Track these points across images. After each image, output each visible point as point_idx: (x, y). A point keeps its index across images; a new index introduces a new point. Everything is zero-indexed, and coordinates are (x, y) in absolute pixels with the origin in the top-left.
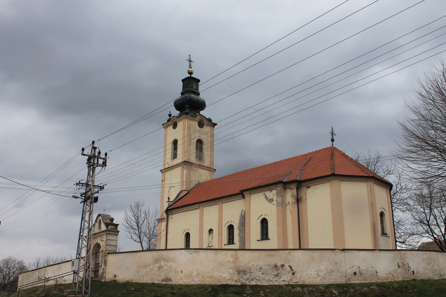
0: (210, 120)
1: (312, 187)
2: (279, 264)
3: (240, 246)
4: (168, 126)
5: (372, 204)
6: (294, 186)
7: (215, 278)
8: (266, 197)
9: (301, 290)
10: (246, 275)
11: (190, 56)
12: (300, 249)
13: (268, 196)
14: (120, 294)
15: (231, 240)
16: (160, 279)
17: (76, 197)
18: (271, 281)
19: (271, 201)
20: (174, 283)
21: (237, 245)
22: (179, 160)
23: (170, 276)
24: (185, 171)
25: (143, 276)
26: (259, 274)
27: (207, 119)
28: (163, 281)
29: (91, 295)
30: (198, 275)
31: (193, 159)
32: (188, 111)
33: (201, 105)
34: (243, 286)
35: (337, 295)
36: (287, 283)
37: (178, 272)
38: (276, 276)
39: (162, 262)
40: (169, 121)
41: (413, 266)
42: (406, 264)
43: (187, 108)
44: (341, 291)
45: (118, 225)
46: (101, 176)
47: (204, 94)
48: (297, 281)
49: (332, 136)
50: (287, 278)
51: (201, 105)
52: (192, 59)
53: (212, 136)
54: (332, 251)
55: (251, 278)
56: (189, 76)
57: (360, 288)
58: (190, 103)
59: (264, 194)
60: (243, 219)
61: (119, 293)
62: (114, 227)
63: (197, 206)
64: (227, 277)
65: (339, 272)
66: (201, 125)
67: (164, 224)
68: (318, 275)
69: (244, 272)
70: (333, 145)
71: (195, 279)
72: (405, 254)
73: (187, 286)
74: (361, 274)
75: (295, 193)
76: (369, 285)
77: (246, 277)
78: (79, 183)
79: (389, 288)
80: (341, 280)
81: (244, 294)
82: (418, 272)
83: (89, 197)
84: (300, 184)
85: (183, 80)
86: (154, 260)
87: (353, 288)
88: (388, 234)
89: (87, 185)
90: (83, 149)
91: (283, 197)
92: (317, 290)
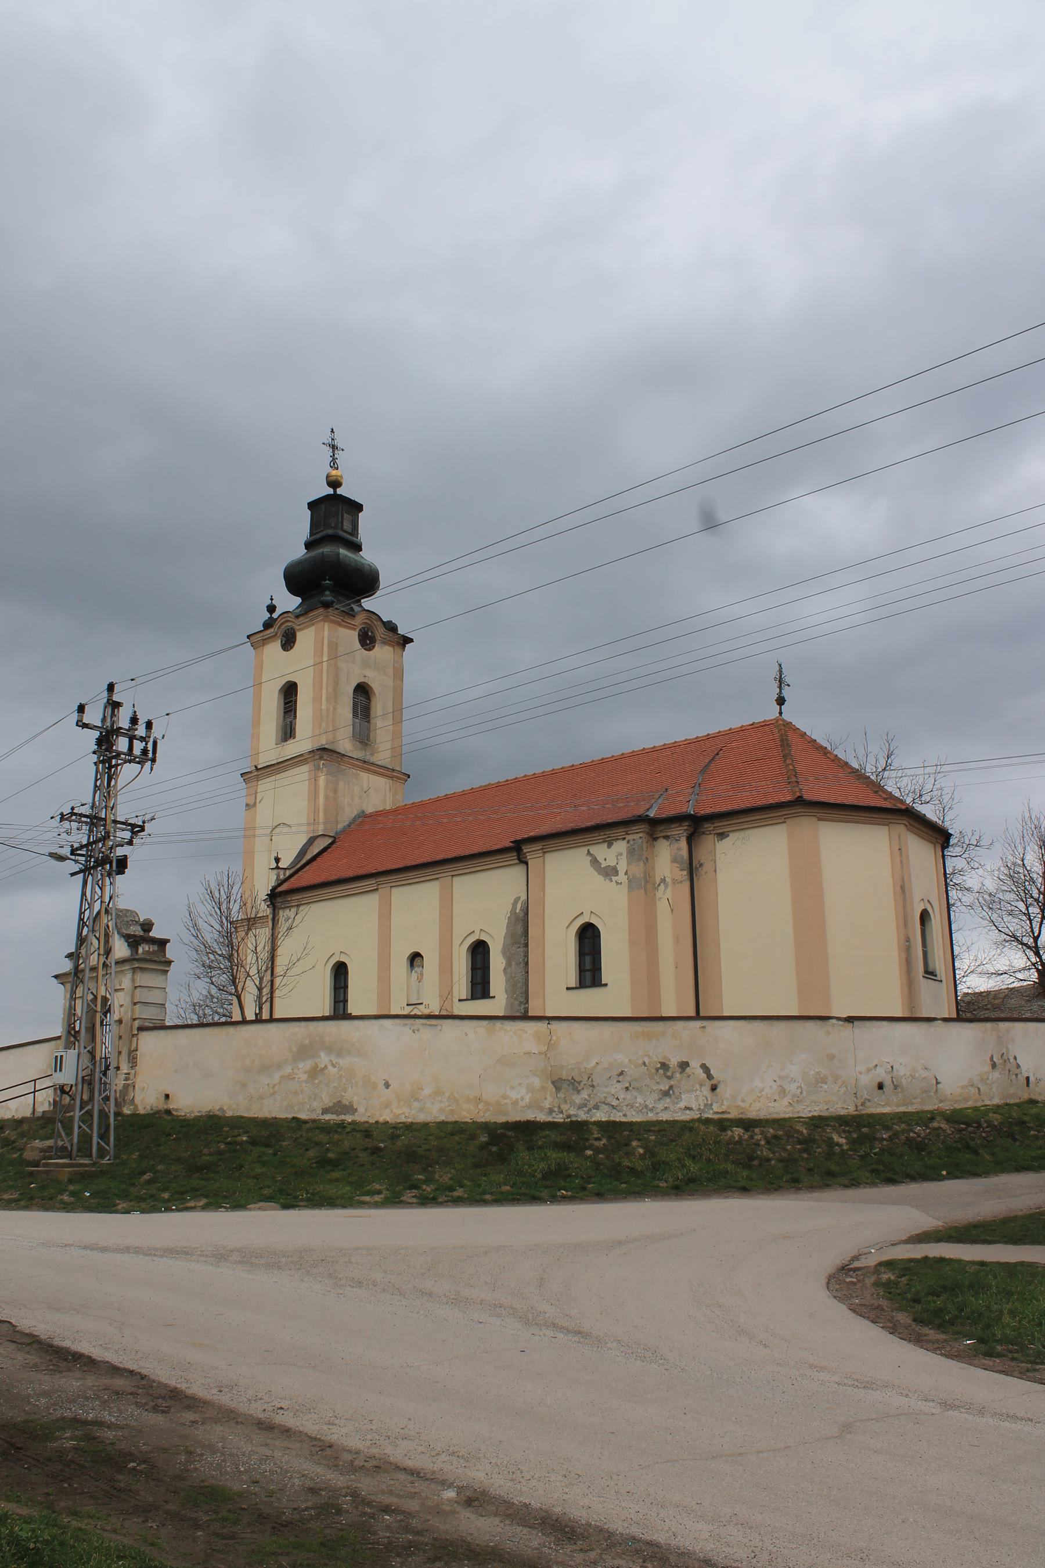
0: (391, 627)
2: (673, 1062)
3: (510, 1005)
4: (265, 641)
5: (902, 888)
6: (680, 832)
7: (487, 1103)
8: (595, 862)
9: (746, 1137)
10: (578, 1092)
11: (332, 431)
12: (698, 1017)
13: (600, 859)
14: (210, 1154)
15: (480, 987)
16: (318, 1105)
17: (61, 858)
18: (651, 1110)
19: (609, 872)
20: (364, 1119)
21: (497, 1003)
22: (303, 742)
23: (350, 1096)
24: (322, 780)
25: (261, 1098)
26: (616, 1088)
27: (383, 623)
28: (325, 1111)
29: (115, 1158)
30: (438, 1093)
31: (346, 745)
32: (330, 598)
33: (366, 582)
34: (578, 1127)
35: (845, 1147)
36: (695, 1115)
37: (375, 1086)
38: (666, 1094)
39: (322, 1055)
40: (268, 625)
41: (1028, 1066)
42: (1012, 1060)
43: (327, 588)
44: (855, 1135)
45: (168, 941)
46: (136, 791)
47: (376, 547)
48: (724, 1108)
49: (780, 687)
50: (697, 1100)
51: (366, 582)
52: (339, 443)
53: (399, 674)
54: (819, 1022)
55: (592, 1103)
56: (331, 491)
57: (903, 1126)
58: (331, 575)
59: (589, 852)
60: (521, 927)
61: (206, 1151)
62: (156, 948)
64: (522, 1099)
65: (839, 1082)
66: (367, 640)
67: (263, 933)
68: (783, 1092)
69: (574, 1085)
70: (781, 713)
71: (428, 1105)
72: (1008, 1031)
73: (409, 1127)
74: (896, 1087)
75: (684, 853)
76: (926, 1118)
77: (578, 1099)
78: (73, 814)
79: (979, 1126)
80: (843, 1106)
81: (586, 1148)
82: (1038, 1081)
83: (100, 853)
84: (697, 826)
85: (312, 505)
86: (295, 1049)
87: (887, 1128)
88: (938, 973)
89: (94, 820)
90: (81, 709)
91: (648, 861)
92: (789, 1135)
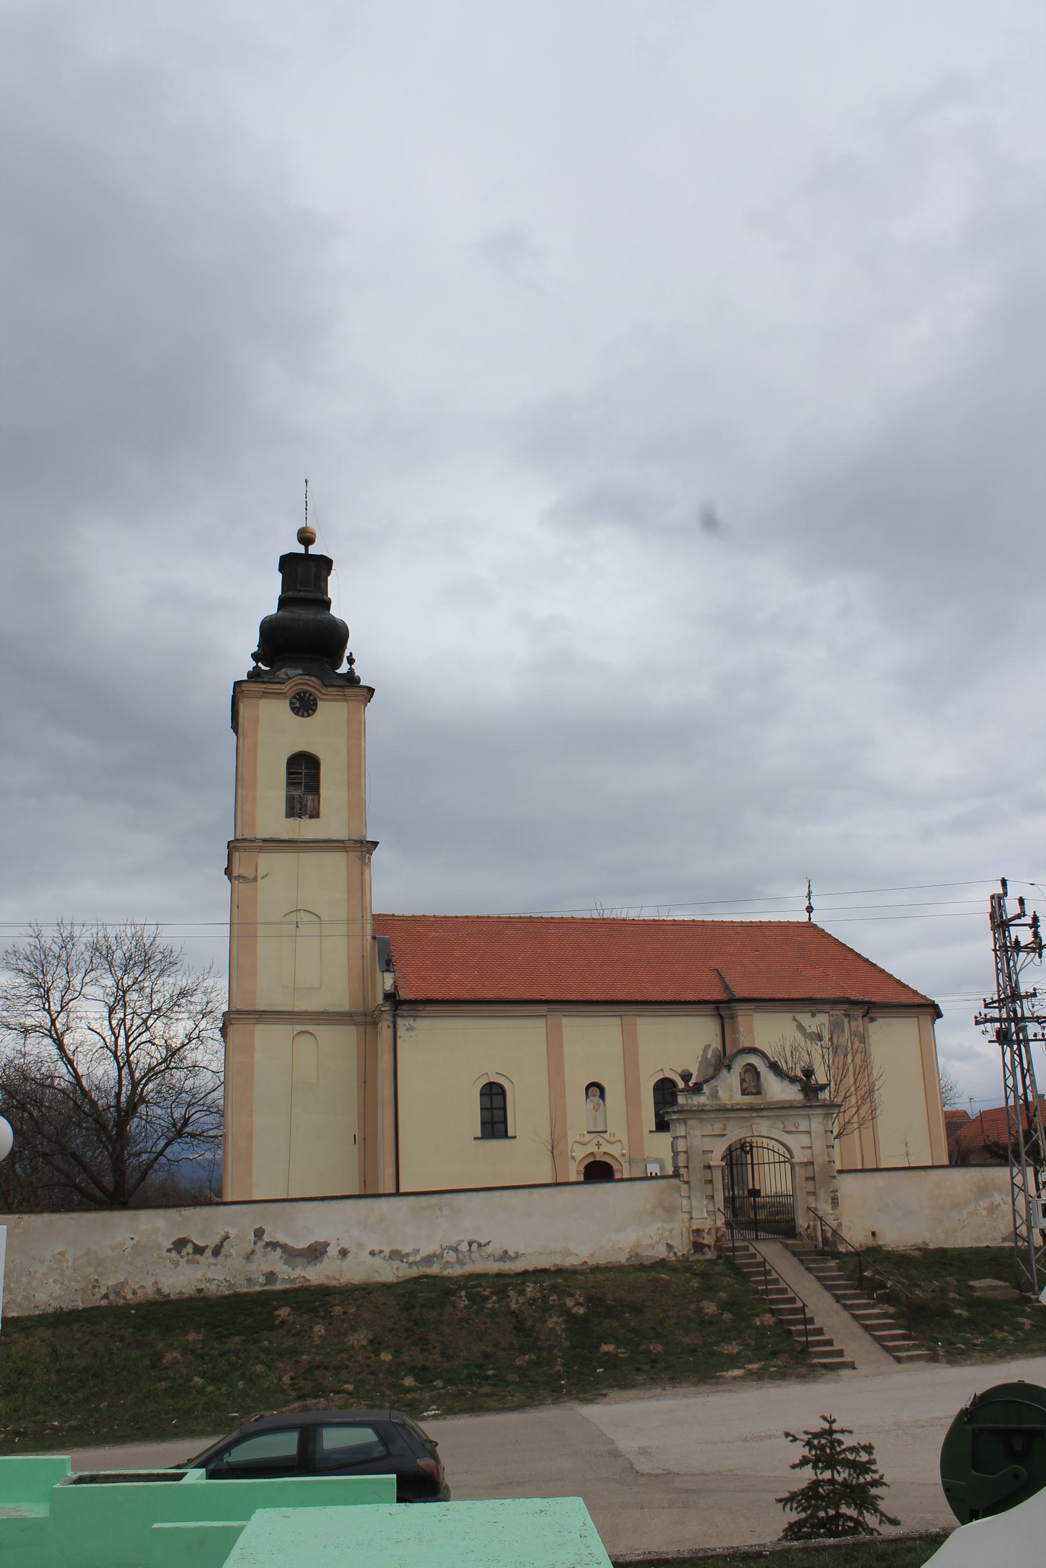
1: (880, 1021)
8: (800, 1027)
16: (998, 1236)
25: (955, 1231)
28: (1004, 1240)
39: (996, 1194)
59: (794, 1019)
63: (543, 1009)
86: (975, 1190)
